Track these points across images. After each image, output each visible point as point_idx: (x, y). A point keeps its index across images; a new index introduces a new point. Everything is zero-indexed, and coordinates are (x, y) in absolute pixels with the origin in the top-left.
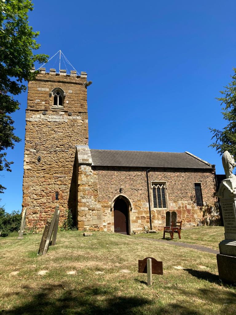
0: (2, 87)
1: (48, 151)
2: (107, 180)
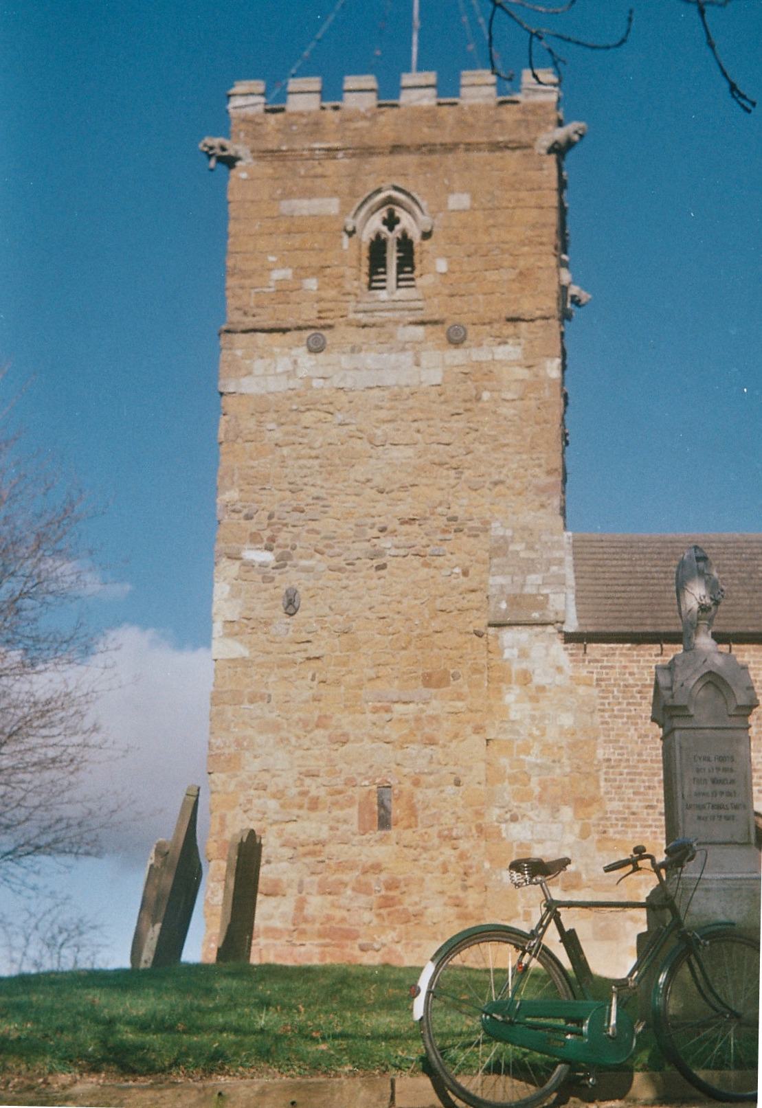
0: (223, 125)
1: (339, 555)
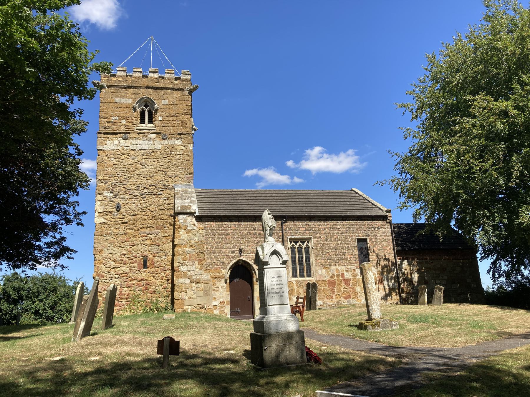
2: (219, 237)
